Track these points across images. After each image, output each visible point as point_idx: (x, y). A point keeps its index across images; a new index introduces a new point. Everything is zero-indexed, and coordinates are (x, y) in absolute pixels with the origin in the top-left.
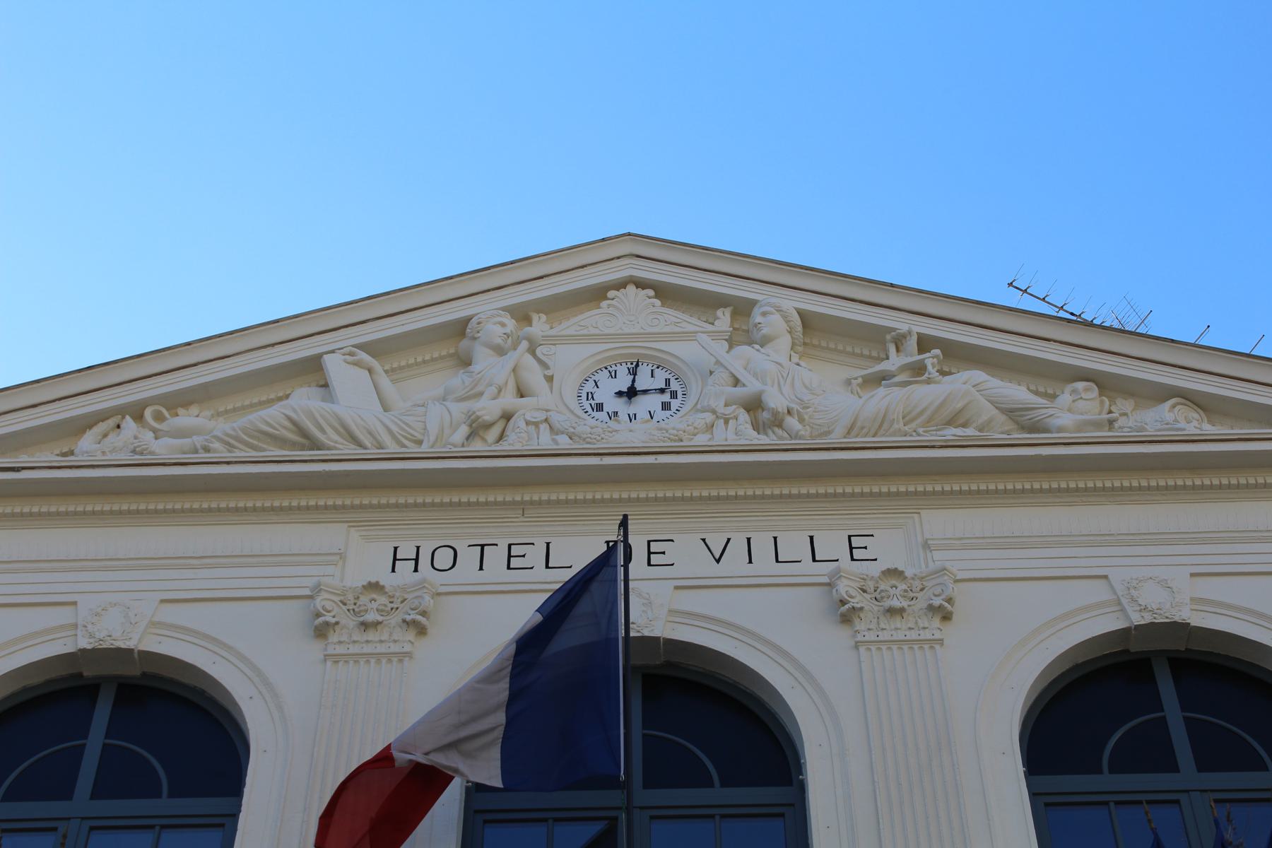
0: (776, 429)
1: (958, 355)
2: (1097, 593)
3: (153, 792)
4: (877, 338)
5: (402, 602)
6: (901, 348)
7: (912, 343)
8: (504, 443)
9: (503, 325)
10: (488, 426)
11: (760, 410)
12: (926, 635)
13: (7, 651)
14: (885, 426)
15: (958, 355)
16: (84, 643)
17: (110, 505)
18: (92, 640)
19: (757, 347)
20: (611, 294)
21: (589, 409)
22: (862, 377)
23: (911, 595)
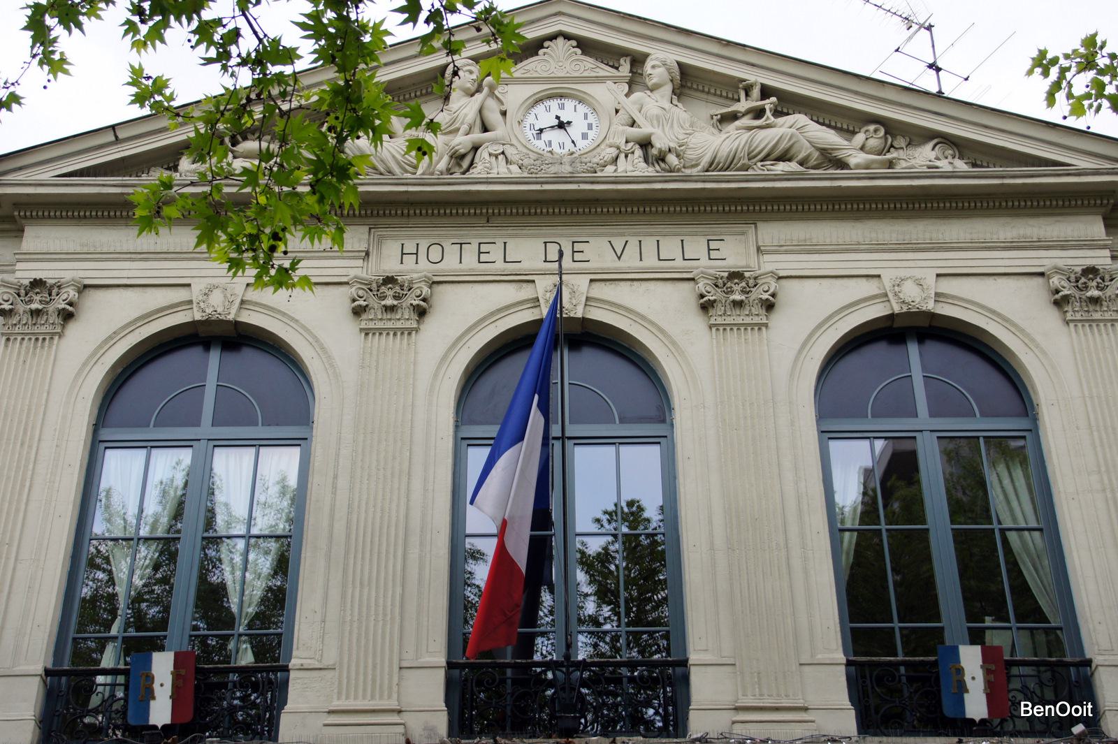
0: (660, 163)
1: (788, 103)
2: (867, 288)
3: (253, 422)
4: (734, 88)
5: (409, 290)
6: (750, 93)
7: (756, 92)
8: (474, 170)
9: (471, 72)
10: (463, 156)
11: (650, 147)
12: (756, 320)
13: (147, 321)
14: (732, 166)
15: (788, 103)
16: (198, 316)
17: (552, 442)
18: (204, 314)
19: (648, 92)
20: (546, 44)
21: (531, 138)
22: (721, 114)
23: (748, 289)
